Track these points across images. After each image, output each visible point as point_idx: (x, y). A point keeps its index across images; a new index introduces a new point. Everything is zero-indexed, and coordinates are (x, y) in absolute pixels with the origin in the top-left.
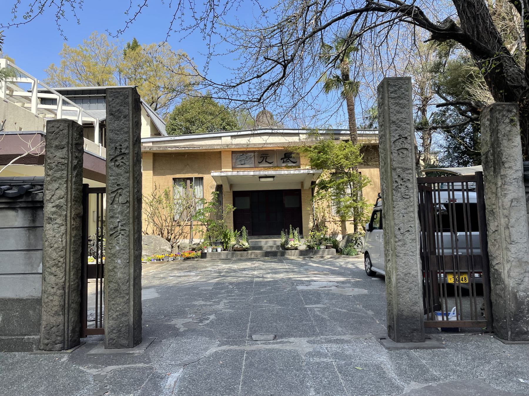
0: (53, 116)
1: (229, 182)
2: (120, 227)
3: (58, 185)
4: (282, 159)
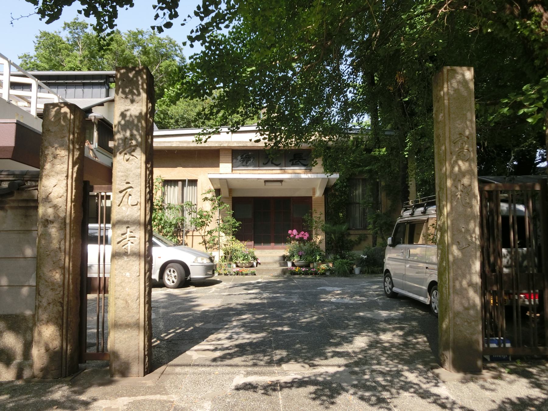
0: (26, 104)
1: (228, 186)
2: (128, 233)
3: (56, 181)
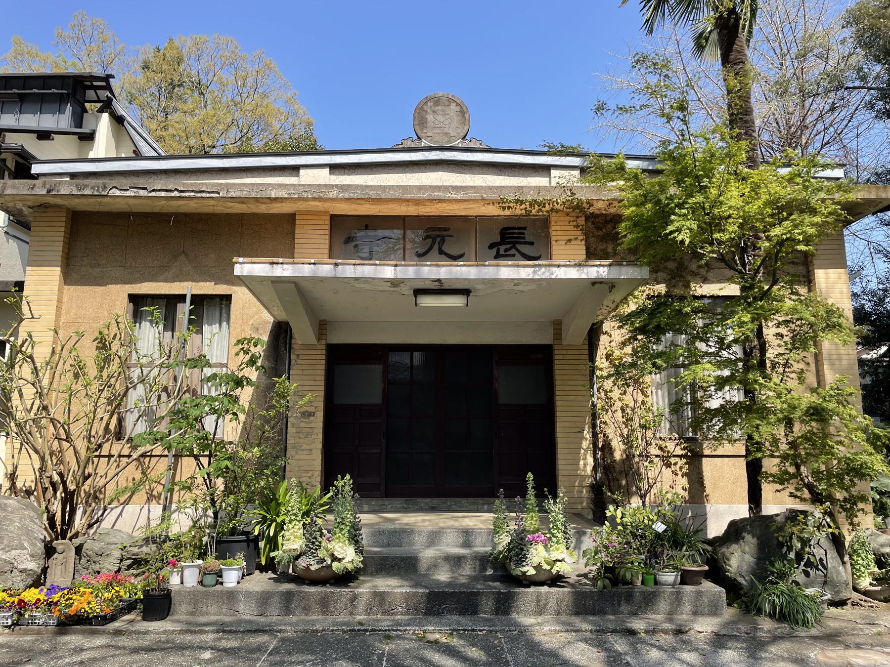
4: (491, 247)
